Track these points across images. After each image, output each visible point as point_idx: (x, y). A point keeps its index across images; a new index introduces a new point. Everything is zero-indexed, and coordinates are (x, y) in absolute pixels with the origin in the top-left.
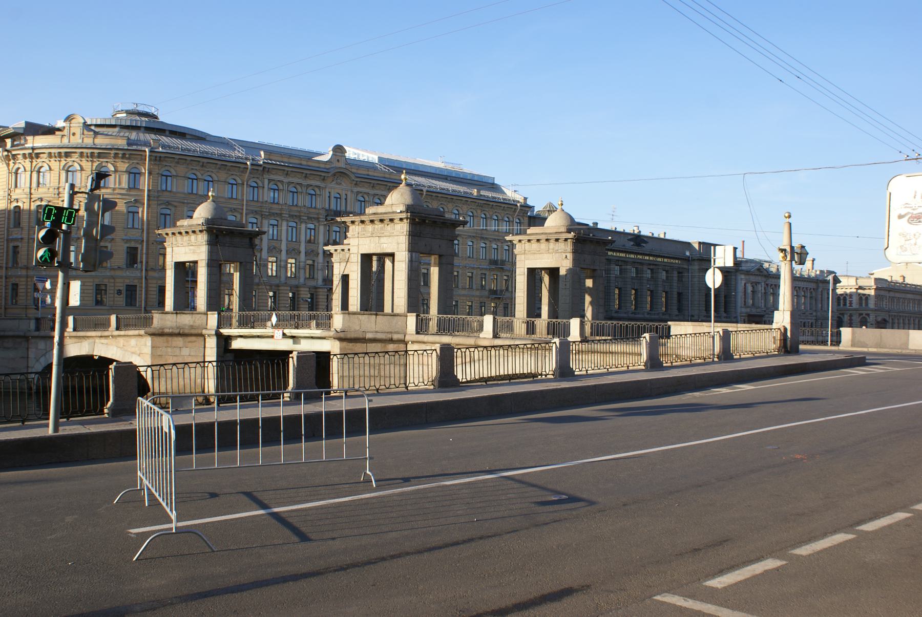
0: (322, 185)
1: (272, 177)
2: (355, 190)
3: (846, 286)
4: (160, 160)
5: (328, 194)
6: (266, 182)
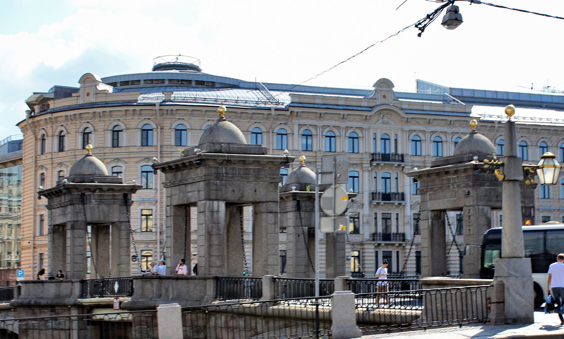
0: (365, 126)
1: (302, 122)
2: (407, 128)
3: (395, 90)
4: (172, 114)
5: (372, 137)
6: (296, 128)
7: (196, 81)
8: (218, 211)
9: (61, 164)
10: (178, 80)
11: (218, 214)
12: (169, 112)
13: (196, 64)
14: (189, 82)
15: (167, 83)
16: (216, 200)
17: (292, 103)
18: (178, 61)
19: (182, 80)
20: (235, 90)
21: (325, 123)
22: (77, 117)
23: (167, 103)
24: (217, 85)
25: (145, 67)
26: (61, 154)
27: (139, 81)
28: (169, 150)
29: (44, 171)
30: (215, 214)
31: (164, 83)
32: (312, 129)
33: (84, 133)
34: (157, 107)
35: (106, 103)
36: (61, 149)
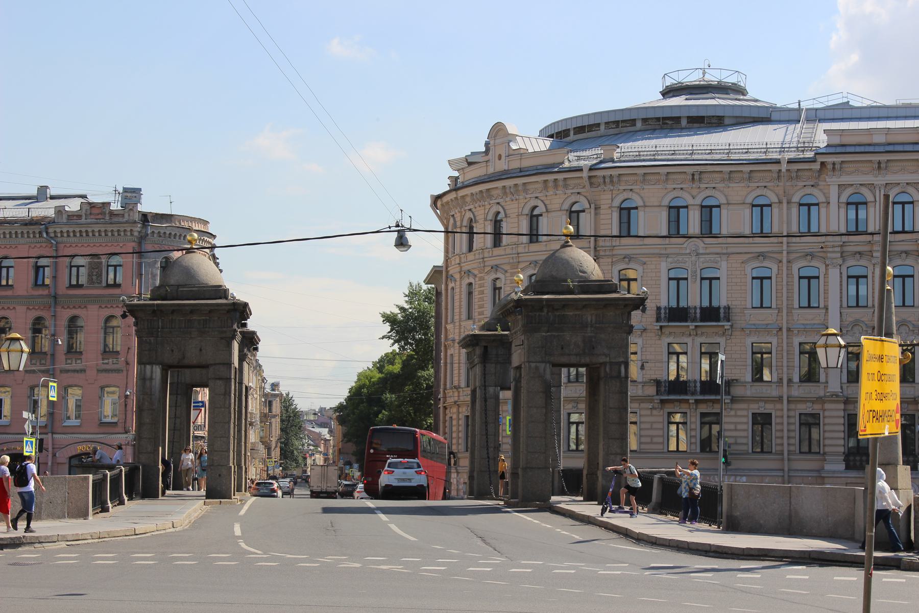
1: (845, 179)
7: (688, 117)
8: (151, 379)
9: (495, 268)
10: (658, 119)
11: (151, 382)
12: (607, 180)
13: (732, 80)
14: (677, 119)
15: (639, 124)
16: (150, 363)
17: (828, 146)
18: (707, 77)
19: (664, 118)
20: (760, 128)
21: (890, 178)
22: (520, 188)
23: (603, 165)
24: (727, 121)
25: (645, 94)
26: (497, 251)
27: (598, 125)
28: (608, 244)
29: (471, 280)
30: (148, 383)
31: (635, 125)
32: (865, 191)
33: (571, 212)
34: (585, 174)
35: (521, 170)
36: (470, 249)
